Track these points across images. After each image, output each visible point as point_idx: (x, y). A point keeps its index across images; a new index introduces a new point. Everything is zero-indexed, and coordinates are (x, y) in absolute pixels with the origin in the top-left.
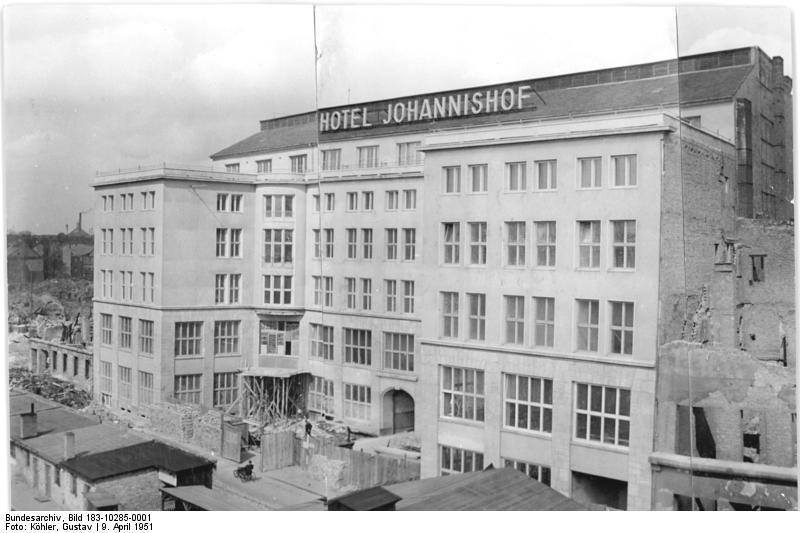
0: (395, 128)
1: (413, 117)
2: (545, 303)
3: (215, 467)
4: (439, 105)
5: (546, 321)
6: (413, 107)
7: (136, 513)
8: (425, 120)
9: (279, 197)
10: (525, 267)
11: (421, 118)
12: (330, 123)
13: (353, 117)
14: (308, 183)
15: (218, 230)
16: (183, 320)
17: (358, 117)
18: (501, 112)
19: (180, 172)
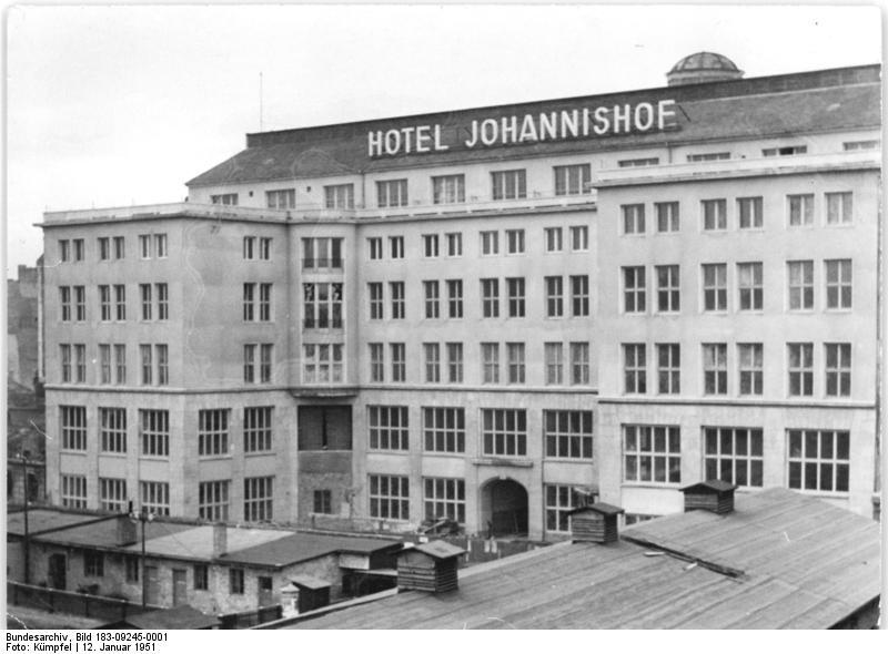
0: (483, 152)
1: (509, 138)
2: (456, 348)
4: (568, 120)
5: (636, 368)
6: (509, 124)
7: (151, 631)
8: (527, 143)
9: (322, 240)
10: (727, 312)
11: (521, 140)
12: (632, 120)
13: (419, 138)
14: (361, 221)
15: (246, 285)
16: (208, 407)
17: (427, 138)
18: (385, 156)
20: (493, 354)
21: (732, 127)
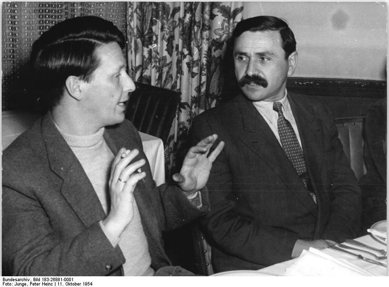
3: (111, 129)
7: (66, 277)
19: (135, 211)
20: (84, 59)
21: (357, 185)
